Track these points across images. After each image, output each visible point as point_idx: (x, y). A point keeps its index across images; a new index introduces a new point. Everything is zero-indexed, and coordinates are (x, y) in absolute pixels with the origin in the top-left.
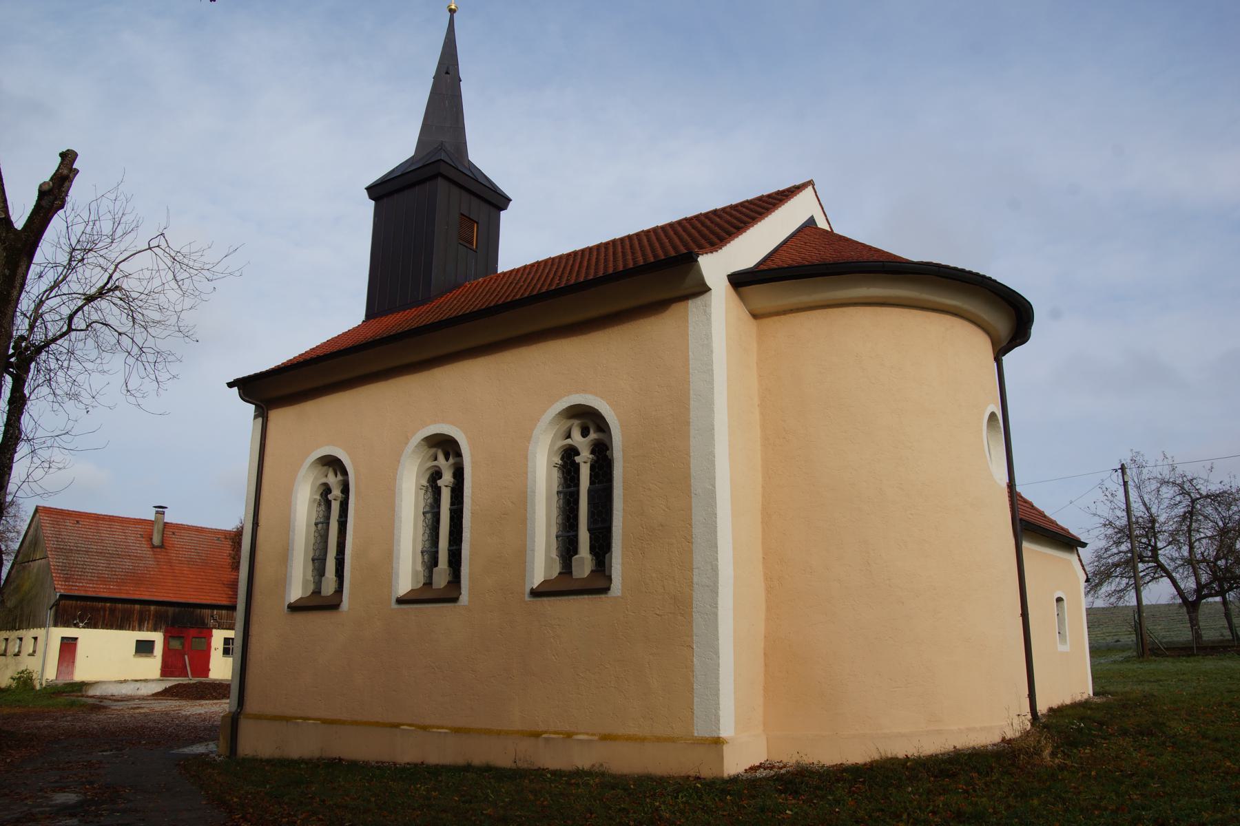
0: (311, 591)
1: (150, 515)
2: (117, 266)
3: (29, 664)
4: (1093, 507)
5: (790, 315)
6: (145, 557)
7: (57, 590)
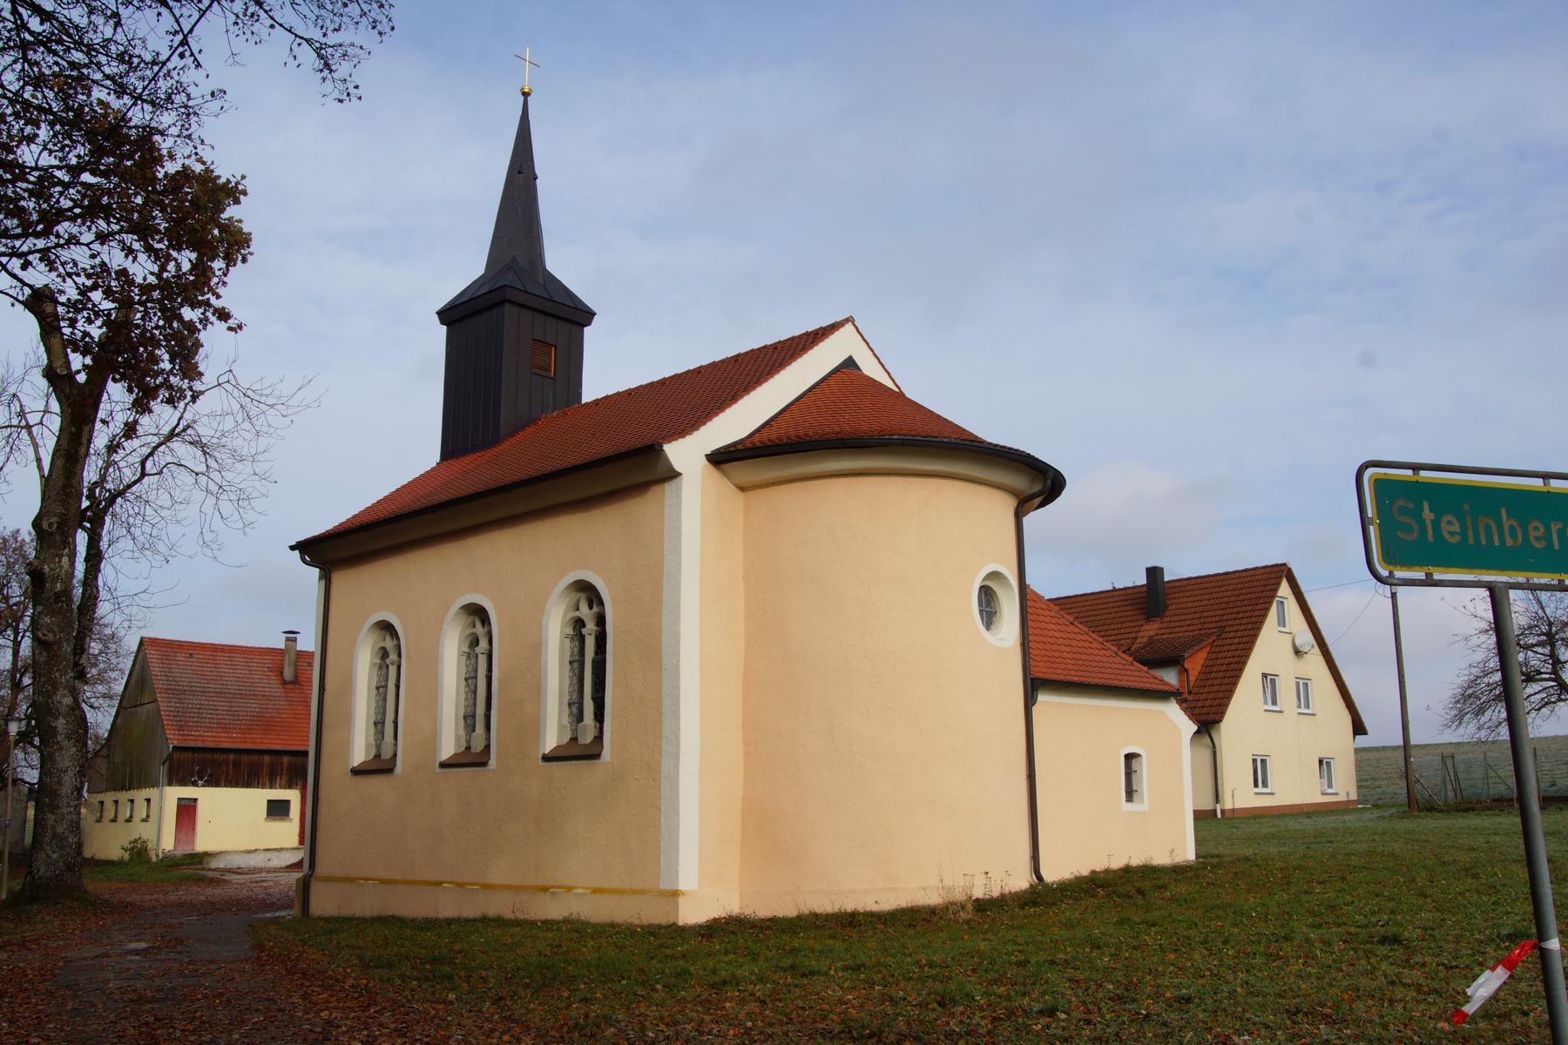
1: (279, 643)
3: (145, 832)
5: (773, 488)
7: (170, 742)
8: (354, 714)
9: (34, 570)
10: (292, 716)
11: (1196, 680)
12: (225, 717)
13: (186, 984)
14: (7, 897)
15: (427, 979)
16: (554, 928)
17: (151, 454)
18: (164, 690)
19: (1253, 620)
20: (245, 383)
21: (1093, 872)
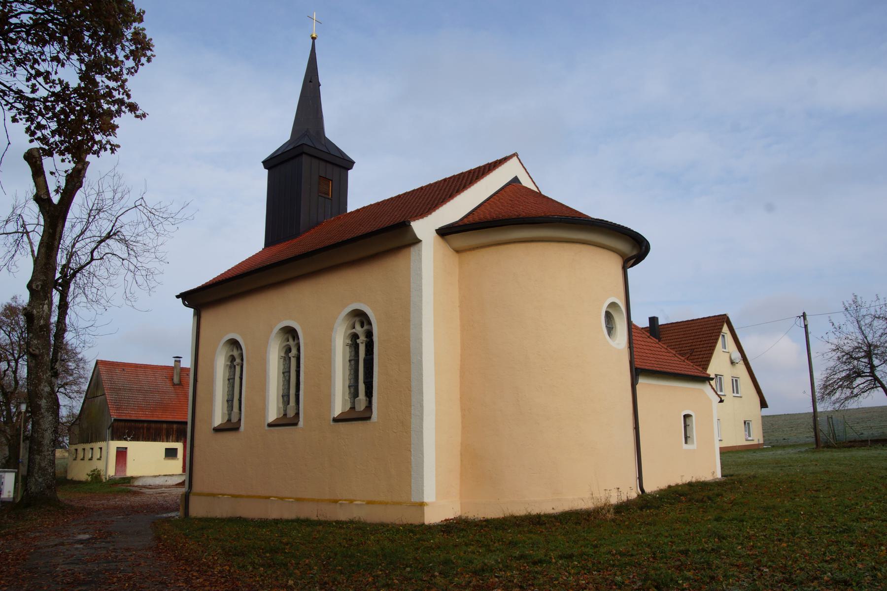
0: (227, 419)
1: (171, 363)
2: (117, 218)
3: (99, 465)
4: (825, 337)
7: (112, 416)
8: (215, 395)
9: (28, 312)
10: (178, 402)
12: (142, 403)
13: (108, 568)
14: (22, 499)
15: (270, 566)
16: (345, 526)
17: (96, 247)
18: (109, 389)
19: (710, 345)
20: (150, 205)
21: (670, 487)
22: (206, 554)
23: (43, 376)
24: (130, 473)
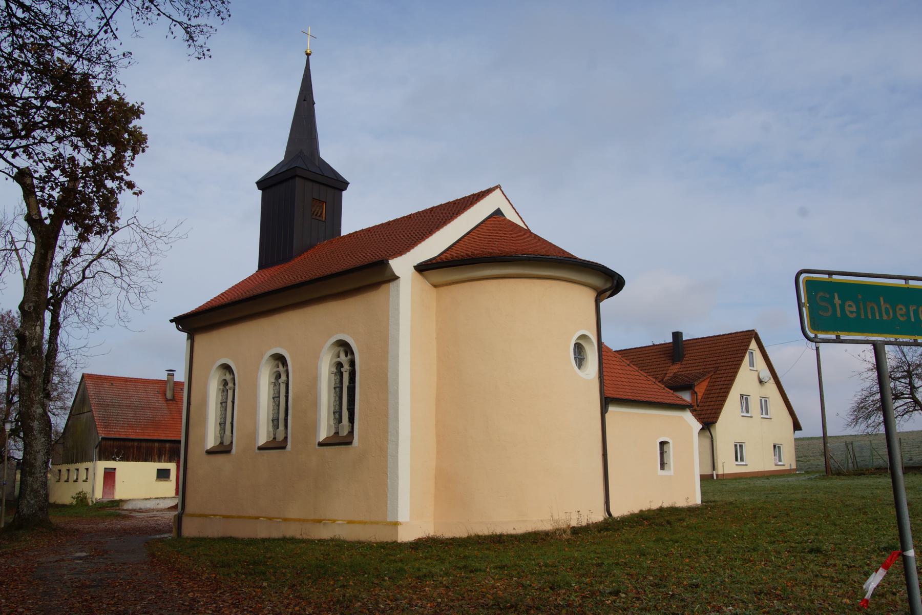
0: (219, 442)
1: (164, 377)
3: (85, 488)
6: (161, 408)
11: (702, 398)
12: (132, 420)
13: (109, 577)
15: (251, 574)
16: (326, 544)
17: (88, 266)
20: (143, 224)
21: (641, 511)
22: (197, 566)
23: (35, 397)
24: (119, 495)
